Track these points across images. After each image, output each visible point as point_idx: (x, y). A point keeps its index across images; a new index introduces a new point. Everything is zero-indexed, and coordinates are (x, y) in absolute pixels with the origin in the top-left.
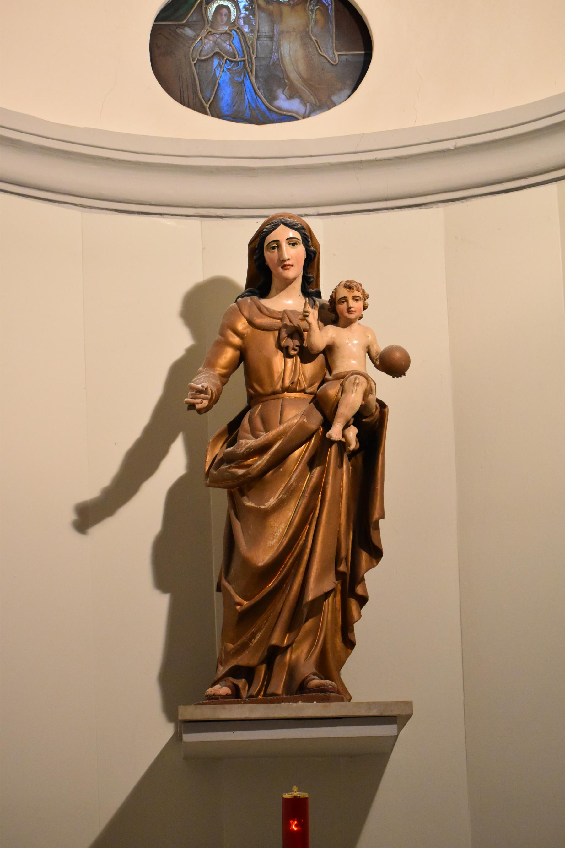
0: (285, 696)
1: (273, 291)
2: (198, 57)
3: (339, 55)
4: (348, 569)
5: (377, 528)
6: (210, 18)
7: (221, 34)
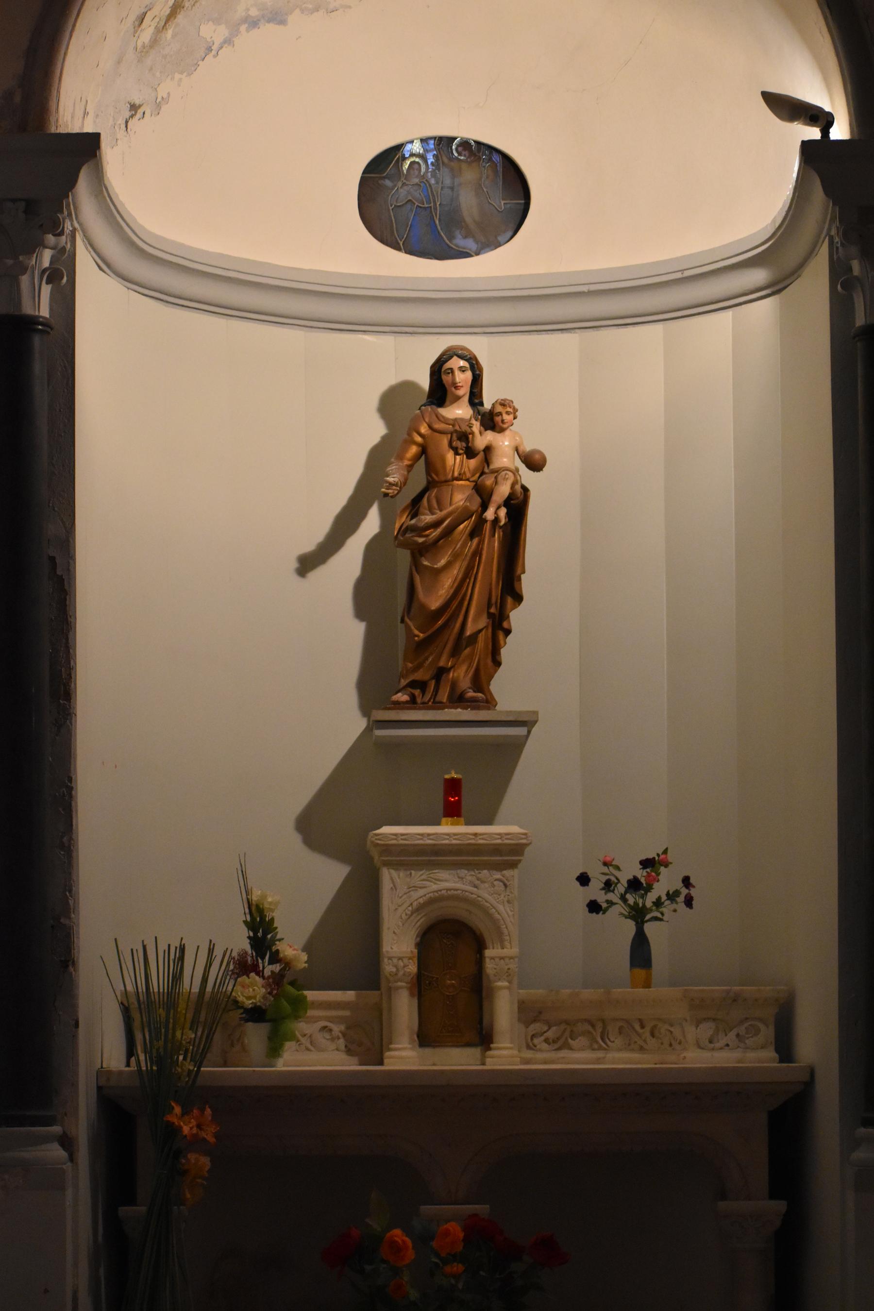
0: (448, 704)
1: (447, 402)
2: (395, 203)
3: (504, 203)
4: (496, 609)
5: (519, 579)
6: (405, 172)
7: (413, 185)
